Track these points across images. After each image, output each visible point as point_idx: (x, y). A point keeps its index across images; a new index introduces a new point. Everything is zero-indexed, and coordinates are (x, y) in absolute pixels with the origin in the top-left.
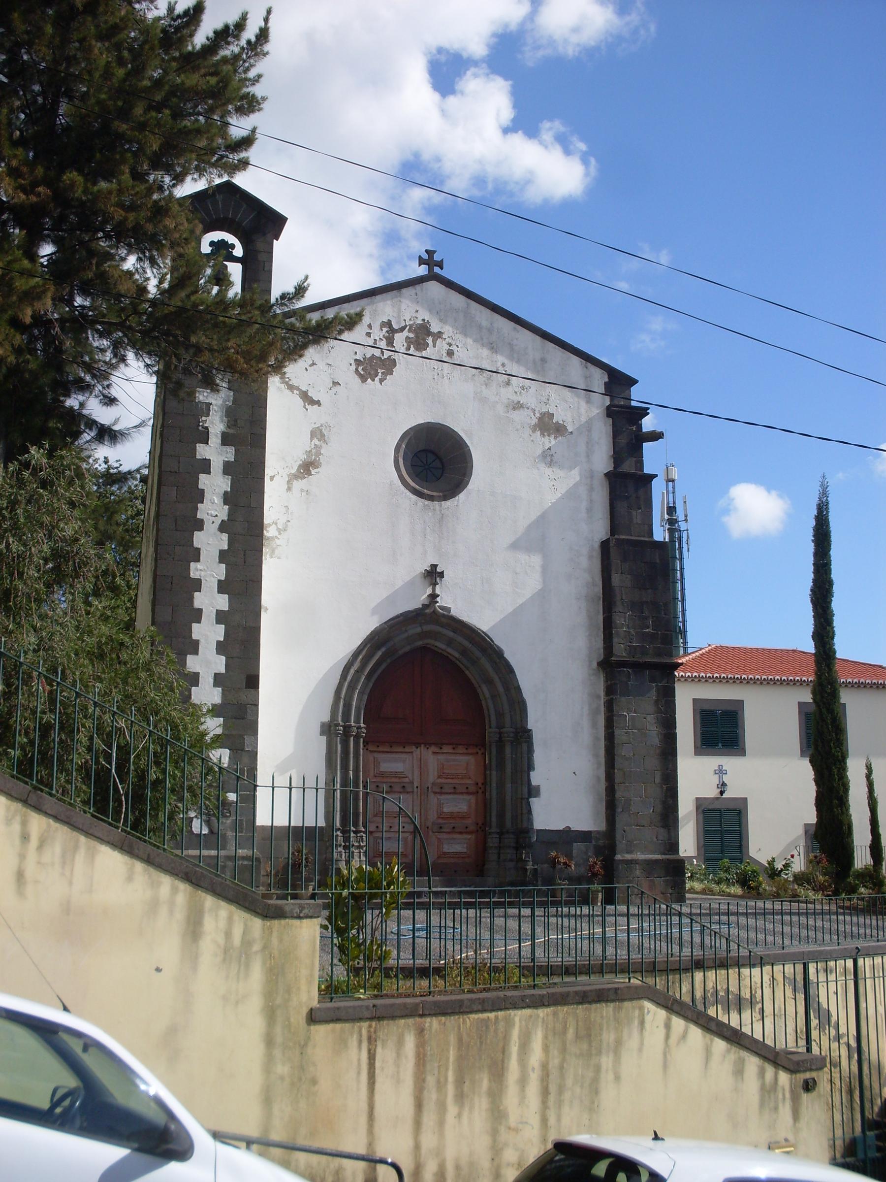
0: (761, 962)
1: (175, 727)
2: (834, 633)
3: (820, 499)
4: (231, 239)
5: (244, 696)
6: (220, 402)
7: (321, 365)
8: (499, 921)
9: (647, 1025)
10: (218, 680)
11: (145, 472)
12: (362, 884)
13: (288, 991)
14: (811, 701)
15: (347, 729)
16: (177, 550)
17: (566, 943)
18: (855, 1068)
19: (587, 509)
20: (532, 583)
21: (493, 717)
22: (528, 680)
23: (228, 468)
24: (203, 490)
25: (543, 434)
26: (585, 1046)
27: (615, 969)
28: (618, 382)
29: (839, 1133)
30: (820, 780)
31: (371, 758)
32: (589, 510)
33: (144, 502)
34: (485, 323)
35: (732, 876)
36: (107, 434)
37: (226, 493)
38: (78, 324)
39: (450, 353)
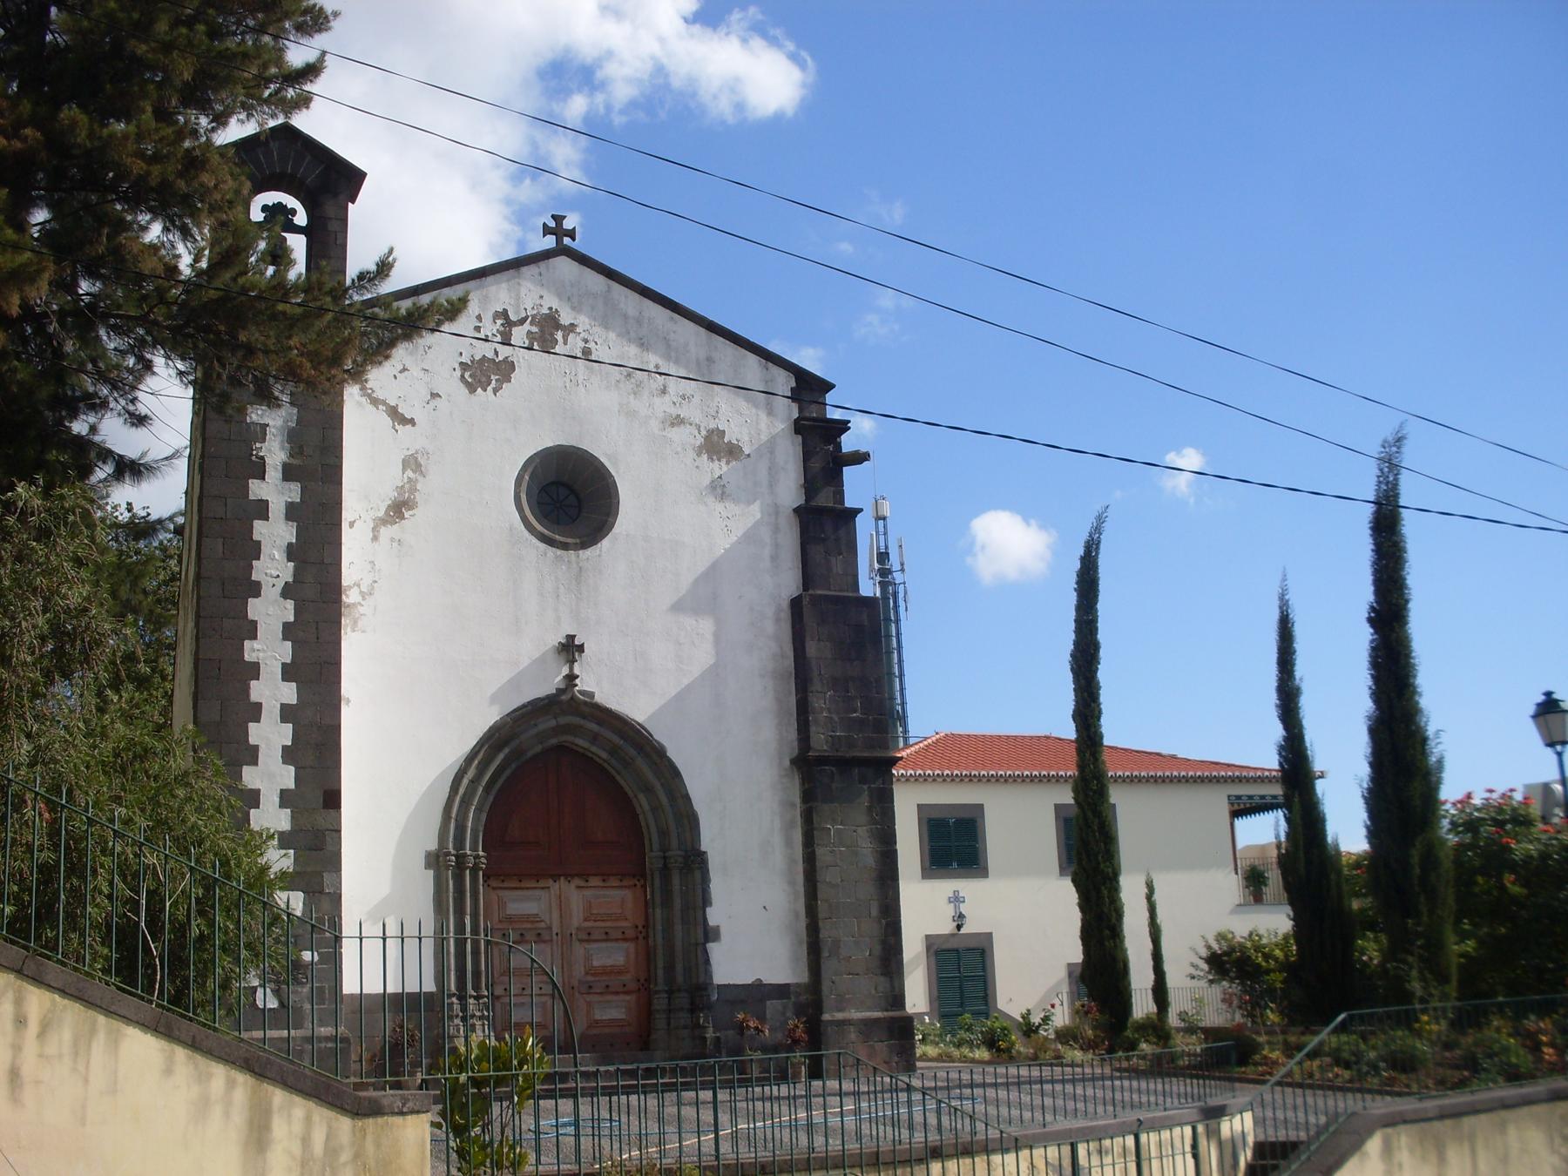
0: (1017, 1145)
1: (225, 863)
2: (1100, 712)
4: (291, 202)
5: (322, 819)
6: (279, 422)
7: (415, 371)
8: (671, 1110)
10: (286, 798)
11: (180, 520)
12: (485, 1064)
15: (461, 858)
16: (226, 624)
17: (760, 1134)
20: (702, 657)
21: (655, 837)
23: (292, 512)
28: (809, 387)
32: (774, 558)
33: (180, 562)
34: (631, 312)
35: (976, 1037)
36: (130, 469)
37: (290, 545)
38: (85, 319)
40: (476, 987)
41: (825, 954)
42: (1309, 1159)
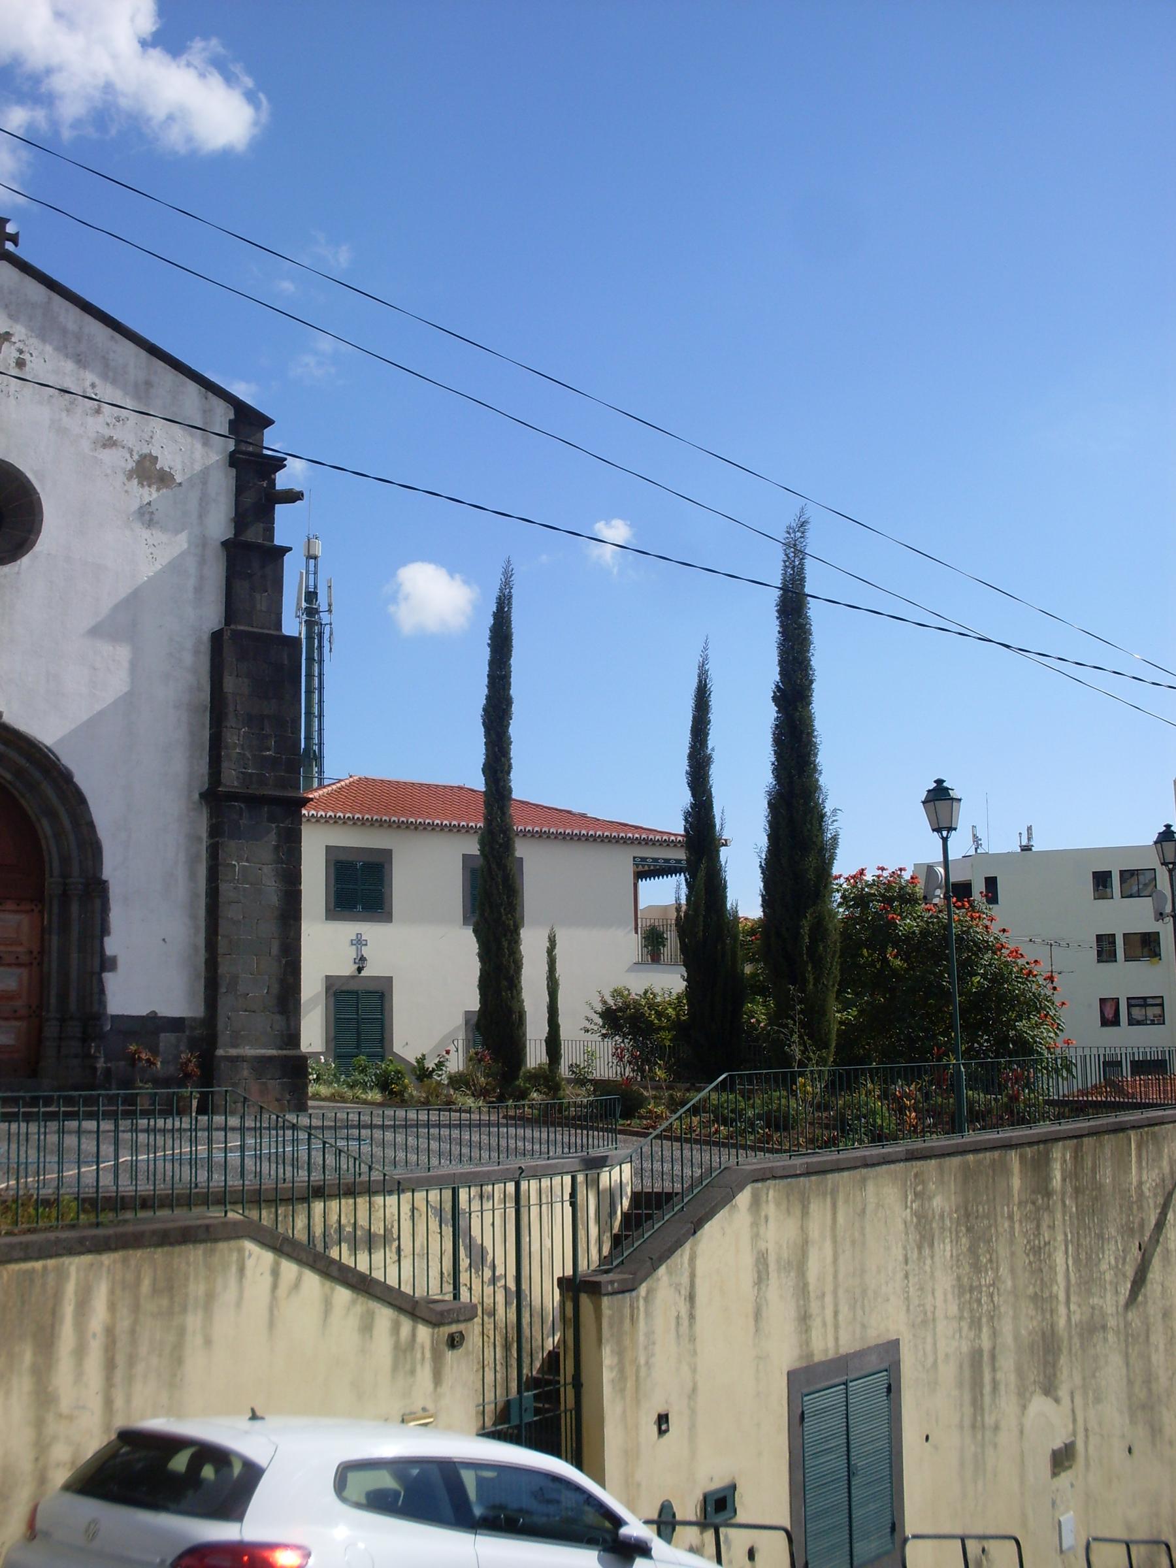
0: (399, 1188)
2: (510, 766)
3: (501, 590)
9: (249, 1272)
14: (478, 853)
18: (513, 1316)
19: (195, 588)
20: (117, 683)
22: (105, 814)
25: (141, 484)
26: (165, 1302)
27: (207, 1199)
28: (248, 421)
29: (490, 1396)
32: (198, 590)
34: (71, 326)
39: (21, 364)
41: (223, 990)
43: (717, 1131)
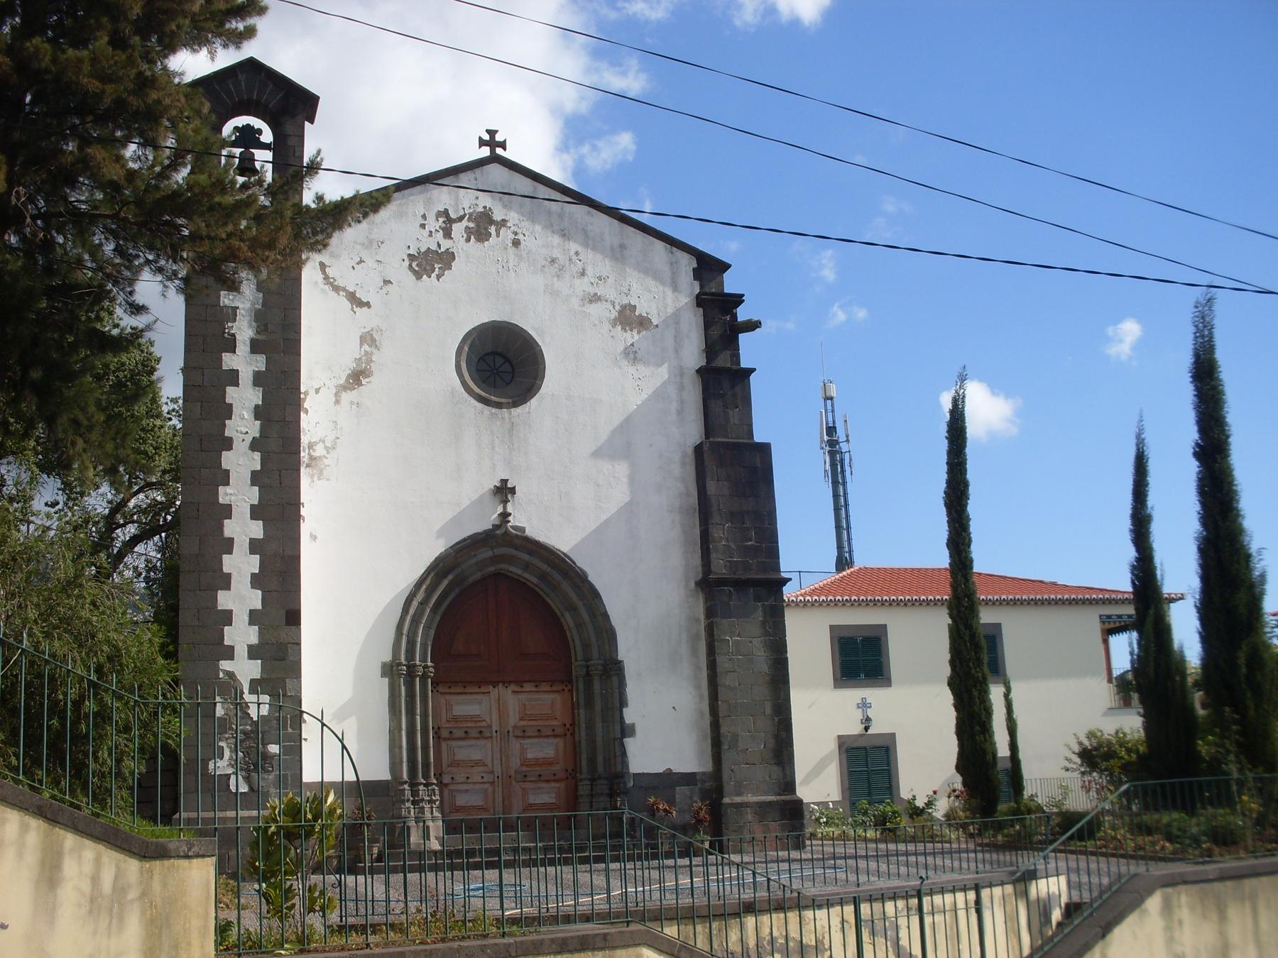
5: (285, 634)
6: (248, 305)
7: (370, 262)
10: (254, 617)
13: (176, 947)
15: (411, 668)
20: (619, 495)
21: (579, 649)
22: (616, 606)
23: (258, 379)
24: (231, 405)
25: (624, 329)
30: (959, 705)
31: (443, 701)
32: (680, 412)
37: (257, 407)
40: (426, 776)
41: (725, 747)
42: (1091, 914)
43: (1163, 848)
